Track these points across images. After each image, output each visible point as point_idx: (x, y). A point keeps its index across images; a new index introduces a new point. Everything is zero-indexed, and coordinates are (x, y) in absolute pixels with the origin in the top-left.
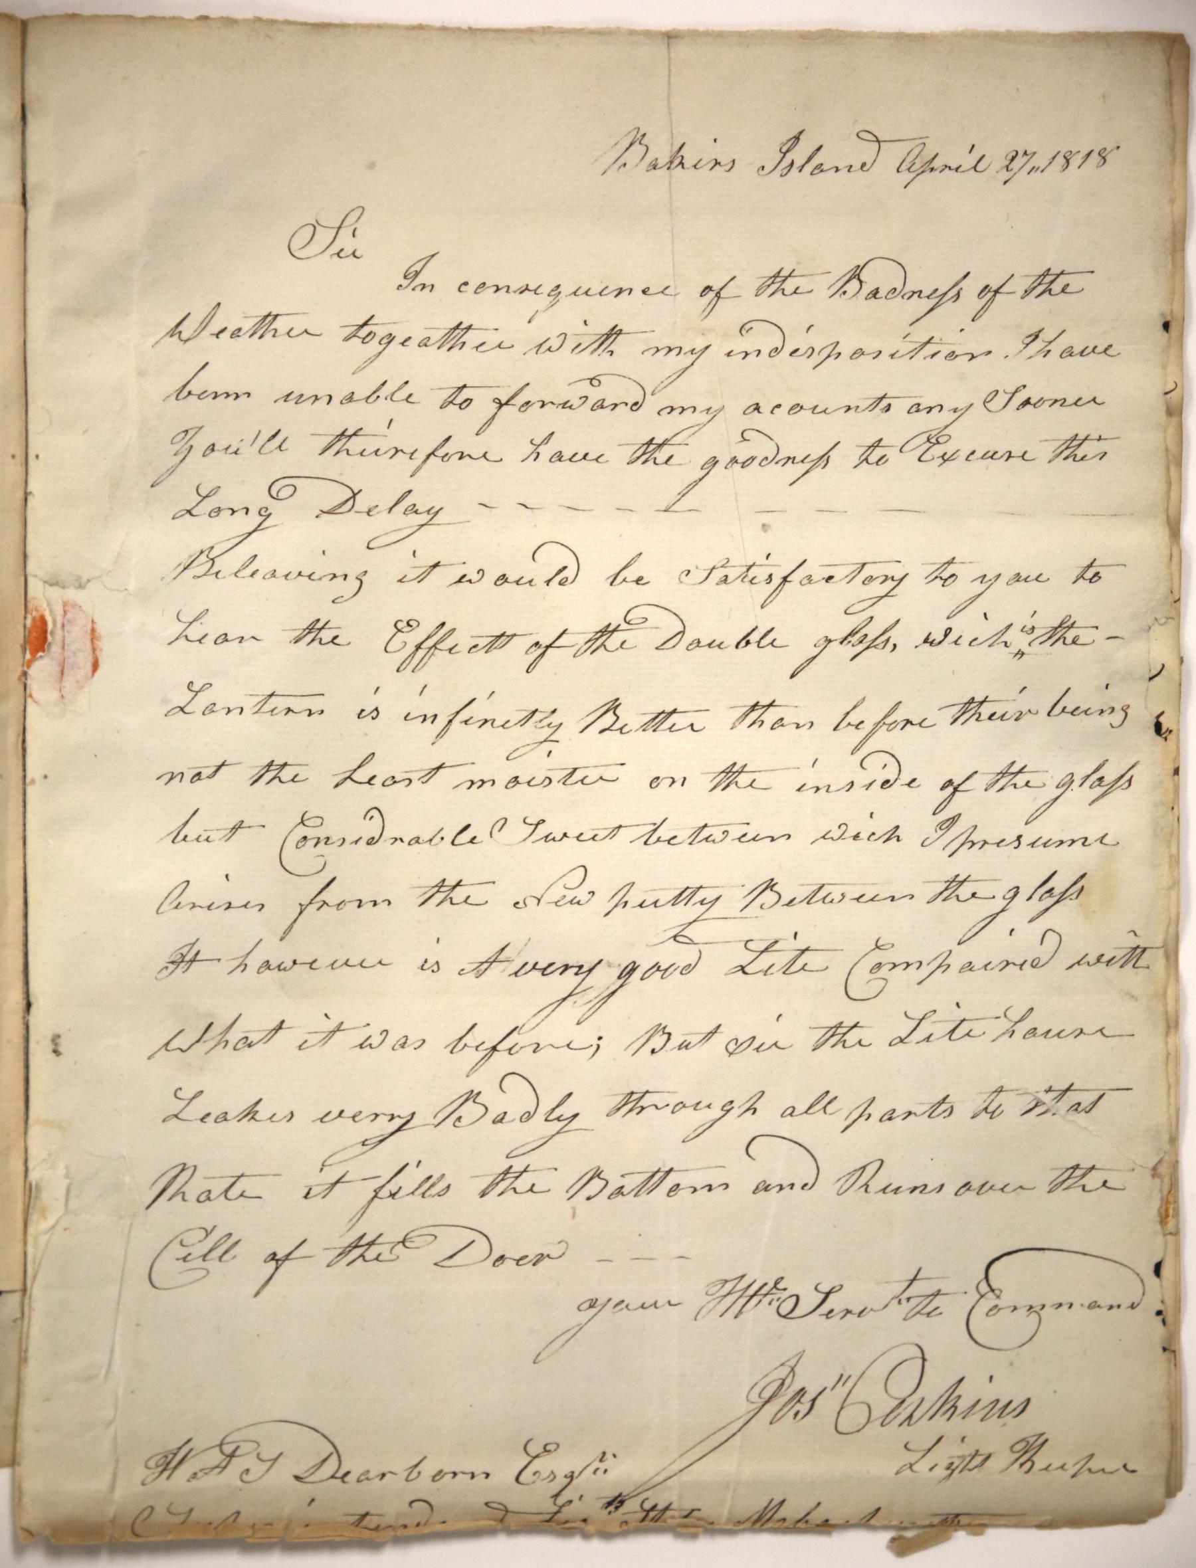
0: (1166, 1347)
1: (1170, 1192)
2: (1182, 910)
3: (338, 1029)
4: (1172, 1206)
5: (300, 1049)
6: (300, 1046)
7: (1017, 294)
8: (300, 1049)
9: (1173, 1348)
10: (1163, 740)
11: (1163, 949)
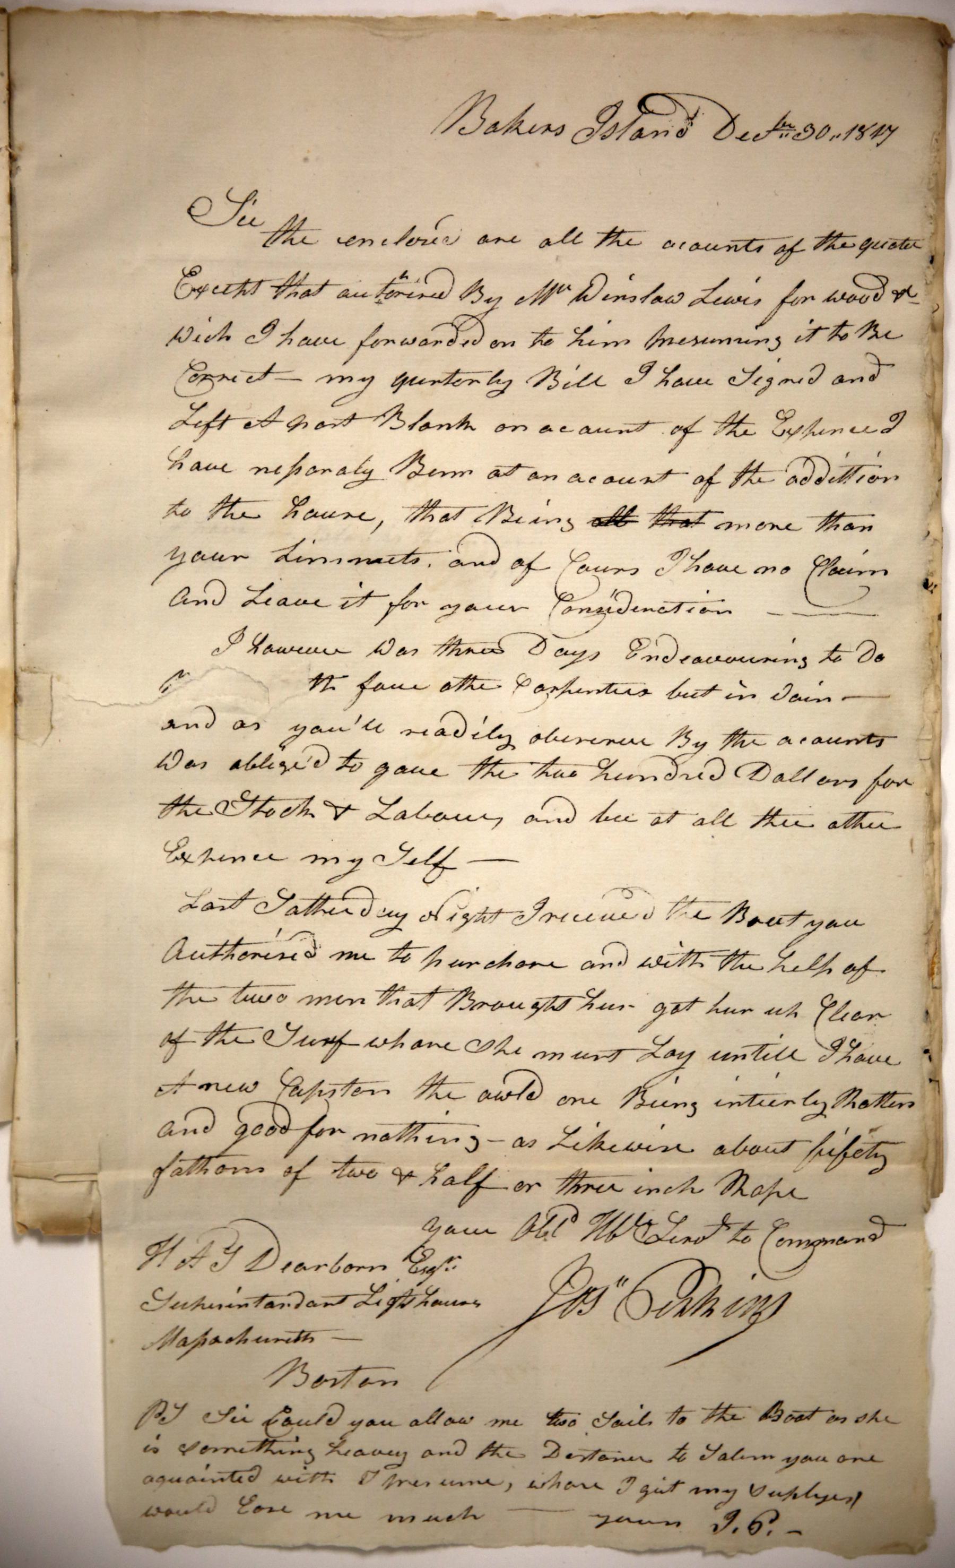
0: (932, 1078)
1: (935, 954)
2: (943, 729)
3: (369, 596)
4: (936, 966)
5: (342, 608)
6: (343, 605)
7: (748, 573)
8: (342, 608)
9: (937, 1079)
10: (930, 593)
11: (929, 761)
